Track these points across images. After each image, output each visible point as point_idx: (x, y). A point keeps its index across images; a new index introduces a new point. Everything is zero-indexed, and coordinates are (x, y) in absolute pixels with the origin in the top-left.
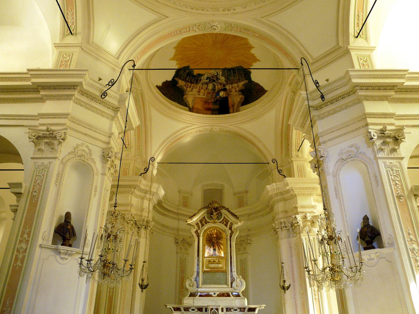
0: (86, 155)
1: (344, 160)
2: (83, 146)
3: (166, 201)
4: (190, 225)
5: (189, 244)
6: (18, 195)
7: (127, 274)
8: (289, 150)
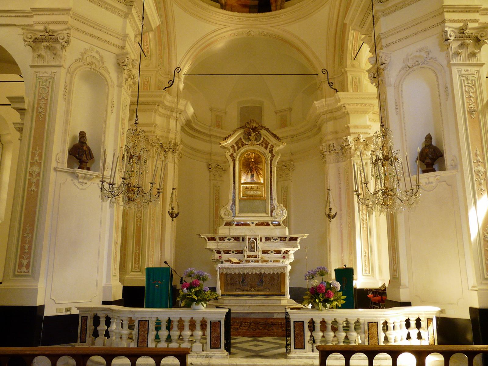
0: (96, 63)
1: (410, 68)
2: (93, 52)
3: (196, 121)
4: (224, 147)
5: (223, 170)
6: (21, 110)
7: (154, 198)
8: (343, 58)
